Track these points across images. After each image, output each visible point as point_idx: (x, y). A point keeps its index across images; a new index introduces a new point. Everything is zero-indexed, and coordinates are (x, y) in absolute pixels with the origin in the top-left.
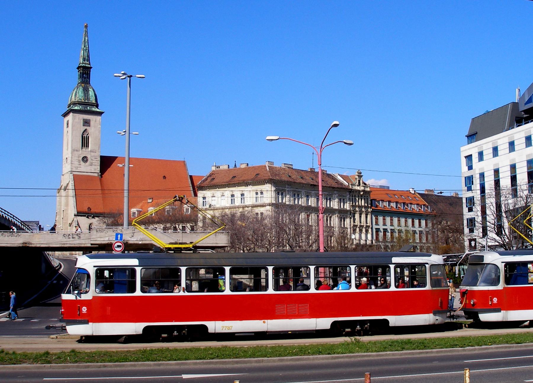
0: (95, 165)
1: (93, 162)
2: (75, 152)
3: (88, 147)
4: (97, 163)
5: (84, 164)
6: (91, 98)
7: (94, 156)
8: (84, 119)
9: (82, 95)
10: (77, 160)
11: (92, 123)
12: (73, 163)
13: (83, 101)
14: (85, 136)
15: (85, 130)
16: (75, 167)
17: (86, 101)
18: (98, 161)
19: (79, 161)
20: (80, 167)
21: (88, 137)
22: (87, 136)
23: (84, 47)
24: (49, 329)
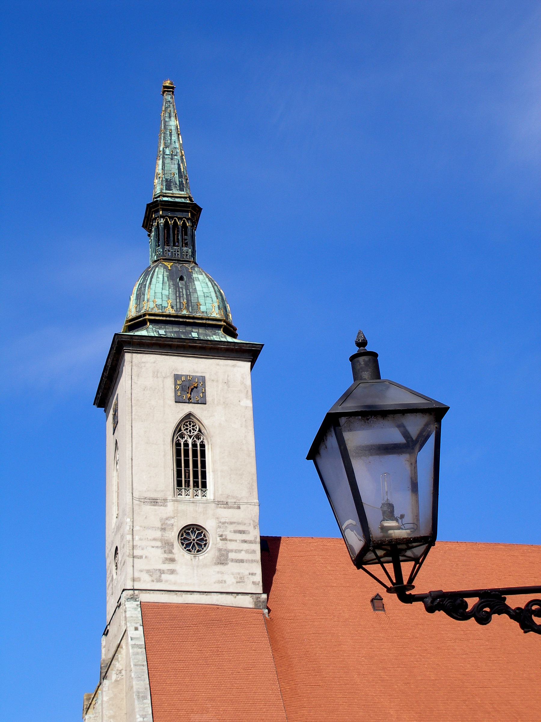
0: (242, 561)
1: (231, 546)
2: (148, 508)
3: (204, 485)
4: (247, 551)
5: (188, 556)
6: (201, 300)
7: (231, 523)
8: (177, 377)
9: (166, 292)
10: (155, 539)
11: (211, 391)
12: (137, 552)
13: (172, 312)
14: (186, 445)
15: (189, 418)
16: (148, 571)
17: (185, 312)
18: (251, 542)
19: (167, 546)
20: (172, 572)
21: (203, 446)
22: (195, 445)
23: (166, 146)
24: (108, 630)
